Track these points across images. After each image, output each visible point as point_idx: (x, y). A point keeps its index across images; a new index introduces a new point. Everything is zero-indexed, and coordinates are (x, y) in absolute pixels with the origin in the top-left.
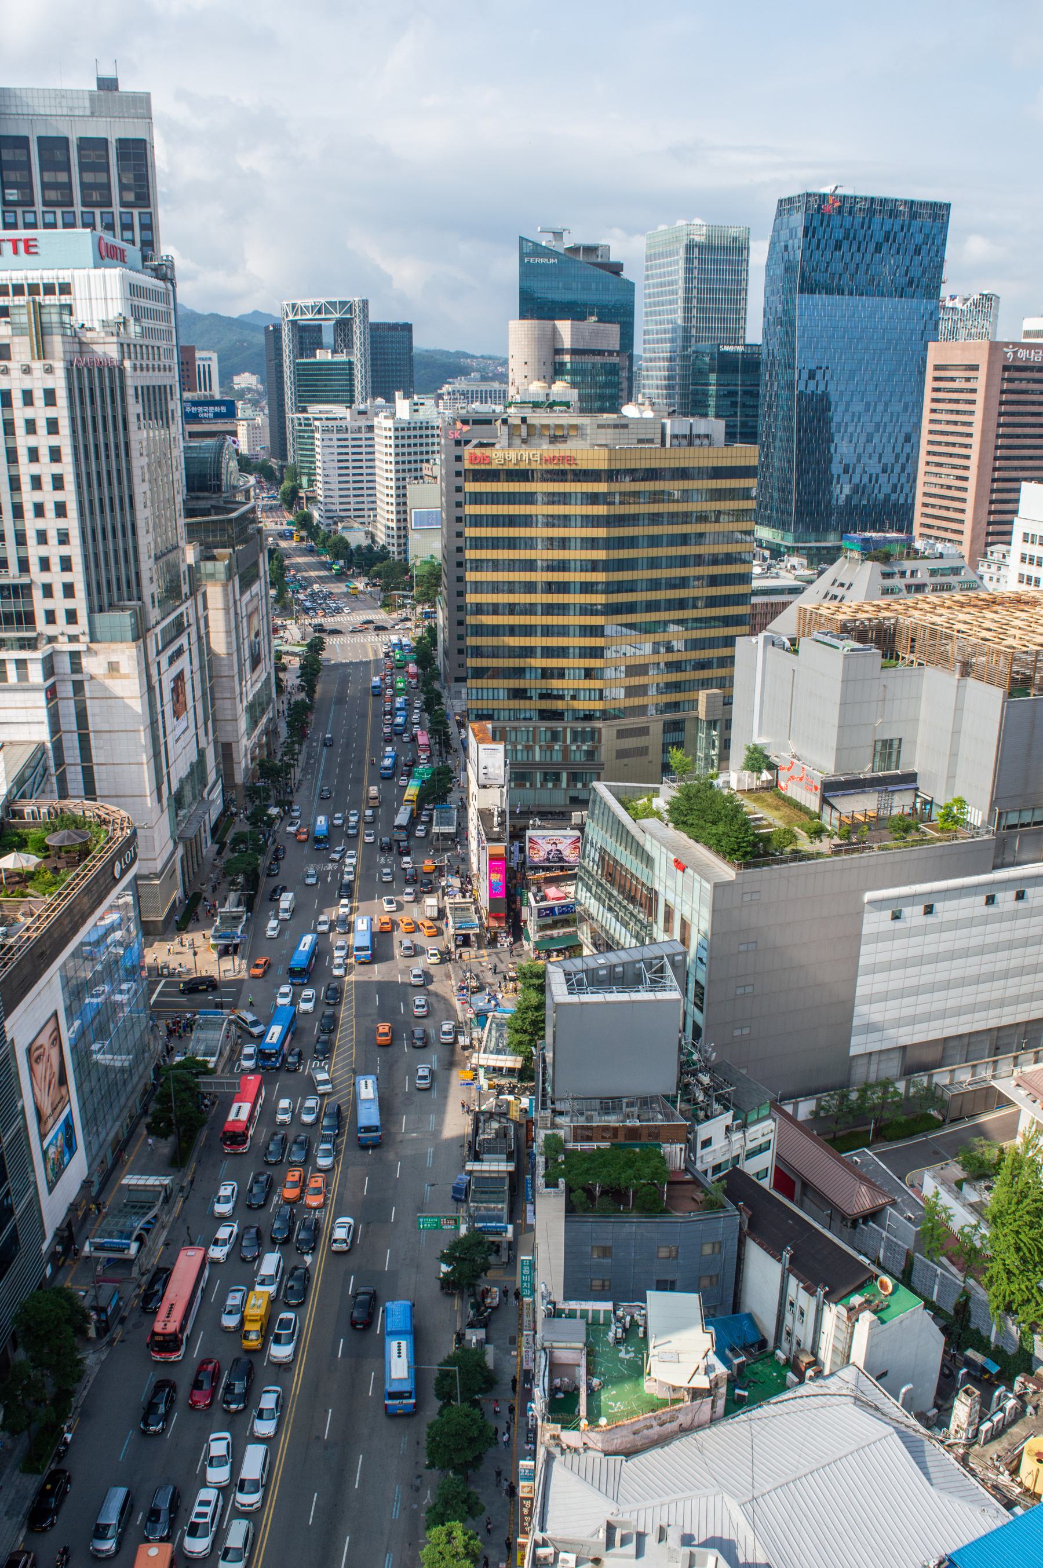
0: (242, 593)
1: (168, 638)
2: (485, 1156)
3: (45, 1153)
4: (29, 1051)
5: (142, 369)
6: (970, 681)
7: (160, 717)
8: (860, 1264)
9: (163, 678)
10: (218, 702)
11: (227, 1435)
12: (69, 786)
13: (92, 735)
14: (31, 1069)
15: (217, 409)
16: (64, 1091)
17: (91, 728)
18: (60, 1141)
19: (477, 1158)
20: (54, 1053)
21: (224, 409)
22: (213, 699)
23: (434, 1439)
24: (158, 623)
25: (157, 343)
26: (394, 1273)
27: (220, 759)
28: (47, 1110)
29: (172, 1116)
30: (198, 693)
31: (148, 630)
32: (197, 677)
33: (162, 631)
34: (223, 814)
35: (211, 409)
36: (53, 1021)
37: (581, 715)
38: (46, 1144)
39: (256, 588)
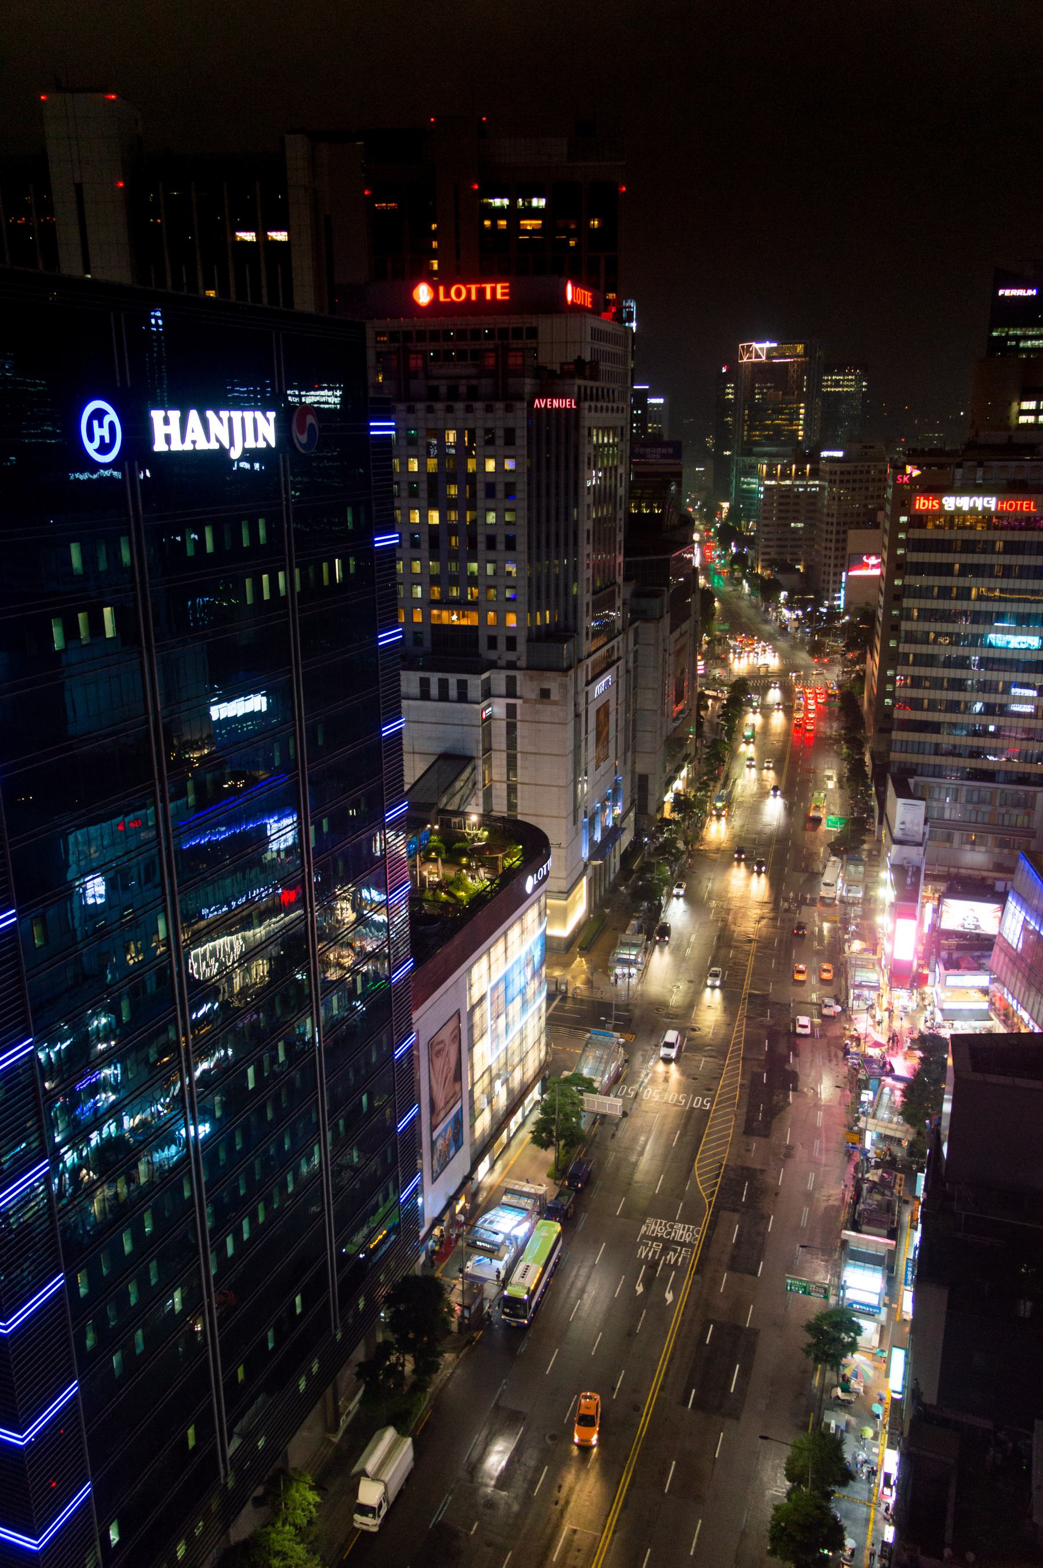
0: (671, 633)
1: (597, 671)
2: (864, 1228)
3: (433, 1144)
4: (430, 1044)
5: (596, 411)
6: (494, 747)
7: (583, 743)
8: (873, 758)
9: (590, 707)
10: (639, 735)
11: (597, 1397)
12: (494, 801)
13: (519, 756)
14: (430, 1061)
15: (664, 451)
16: (457, 1087)
17: (519, 749)
18: (449, 1134)
19: (856, 1227)
20: (453, 1050)
21: (671, 451)
22: (634, 730)
23: (779, 1524)
24: (589, 656)
25: (612, 386)
26: (754, 1332)
27: (636, 790)
28: (440, 1103)
29: (554, 1128)
30: (621, 724)
31: (580, 661)
32: (622, 708)
33: (593, 663)
34: (632, 844)
35: (659, 450)
36: (456, 1018)
37: (1014, 778)
38: (435, 1134)
39: (684, 627)
